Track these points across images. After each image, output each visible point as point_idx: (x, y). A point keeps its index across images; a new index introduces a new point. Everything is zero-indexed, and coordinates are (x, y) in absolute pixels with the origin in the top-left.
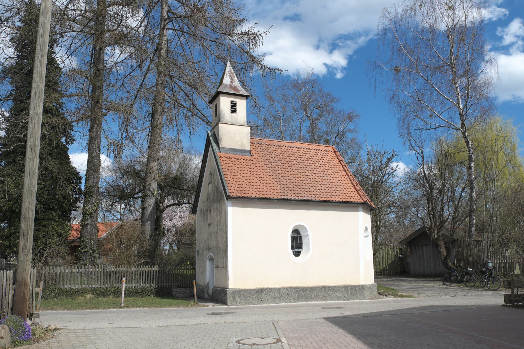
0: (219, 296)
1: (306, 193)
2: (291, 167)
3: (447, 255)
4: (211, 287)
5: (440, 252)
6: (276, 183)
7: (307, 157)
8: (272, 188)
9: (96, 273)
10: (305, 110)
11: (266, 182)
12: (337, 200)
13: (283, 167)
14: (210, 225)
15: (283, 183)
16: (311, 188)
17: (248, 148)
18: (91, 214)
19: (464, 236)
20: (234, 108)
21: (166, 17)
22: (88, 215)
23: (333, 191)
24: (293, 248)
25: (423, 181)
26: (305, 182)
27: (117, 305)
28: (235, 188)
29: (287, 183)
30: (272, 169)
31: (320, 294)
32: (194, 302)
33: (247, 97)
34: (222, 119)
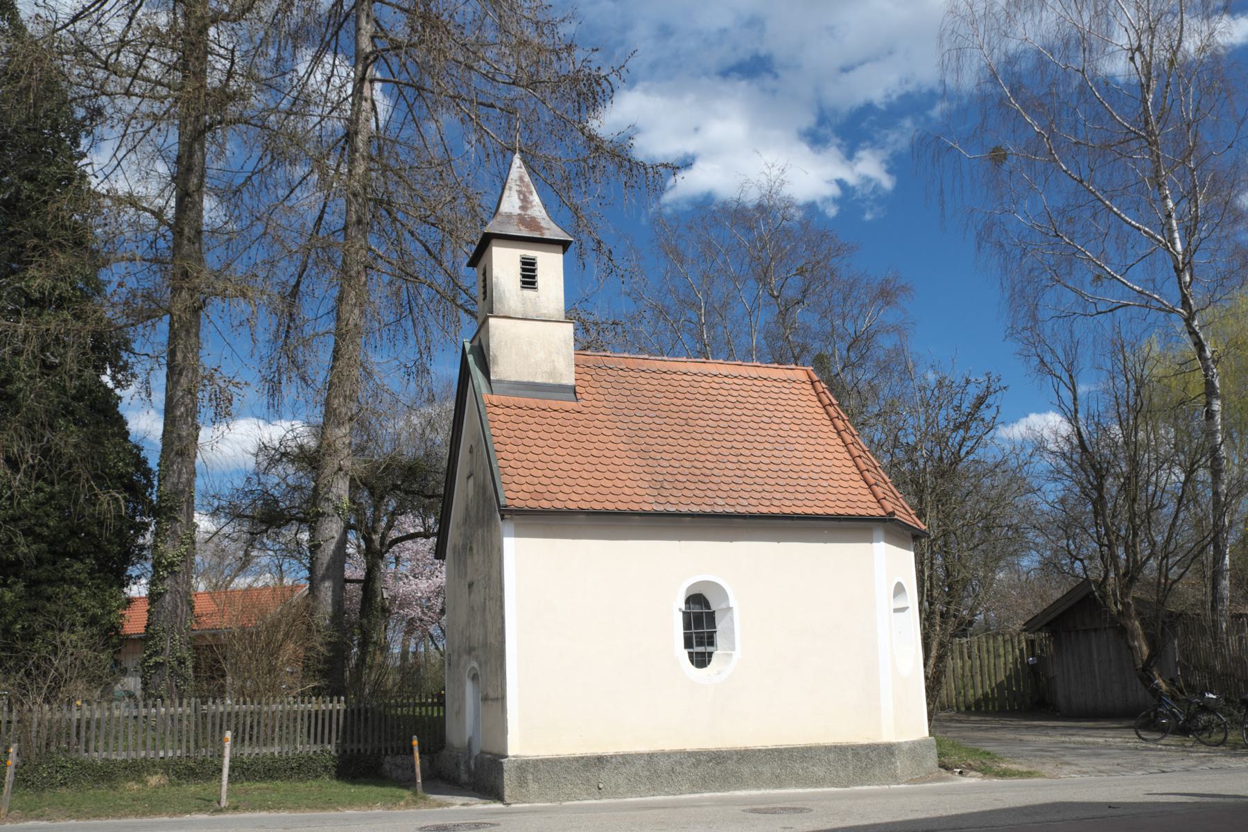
0: (482, 776)
1: (724, 495)
2: (686, 428)
3: (1151, 657)
4: (476, 752)
5: (1131, 648)
6: (640, 470)
7: (733, 399)
8: (629, 483)
9: (241, 714)
10: (763, 278)
11: (611, 467)
12: (809, 511)
13: (664, 427)
14: (471, 585)
15: (659, 469)
16: (736, 480)
17: (569, 379)
18: (172, 564)
19: (1203, 603)
20: (529, 276)
21: (369, 49)
22: (166, 568)
23: (799, 488)
24: (688, 644)
25: (1086, 460)
26: (722, 466)
27: (209, 804)
28: (525, 487)
29: (670, 470)
30: (633, 434)
32: (415, 793)
33: (564, 245)
34: (496, 306)
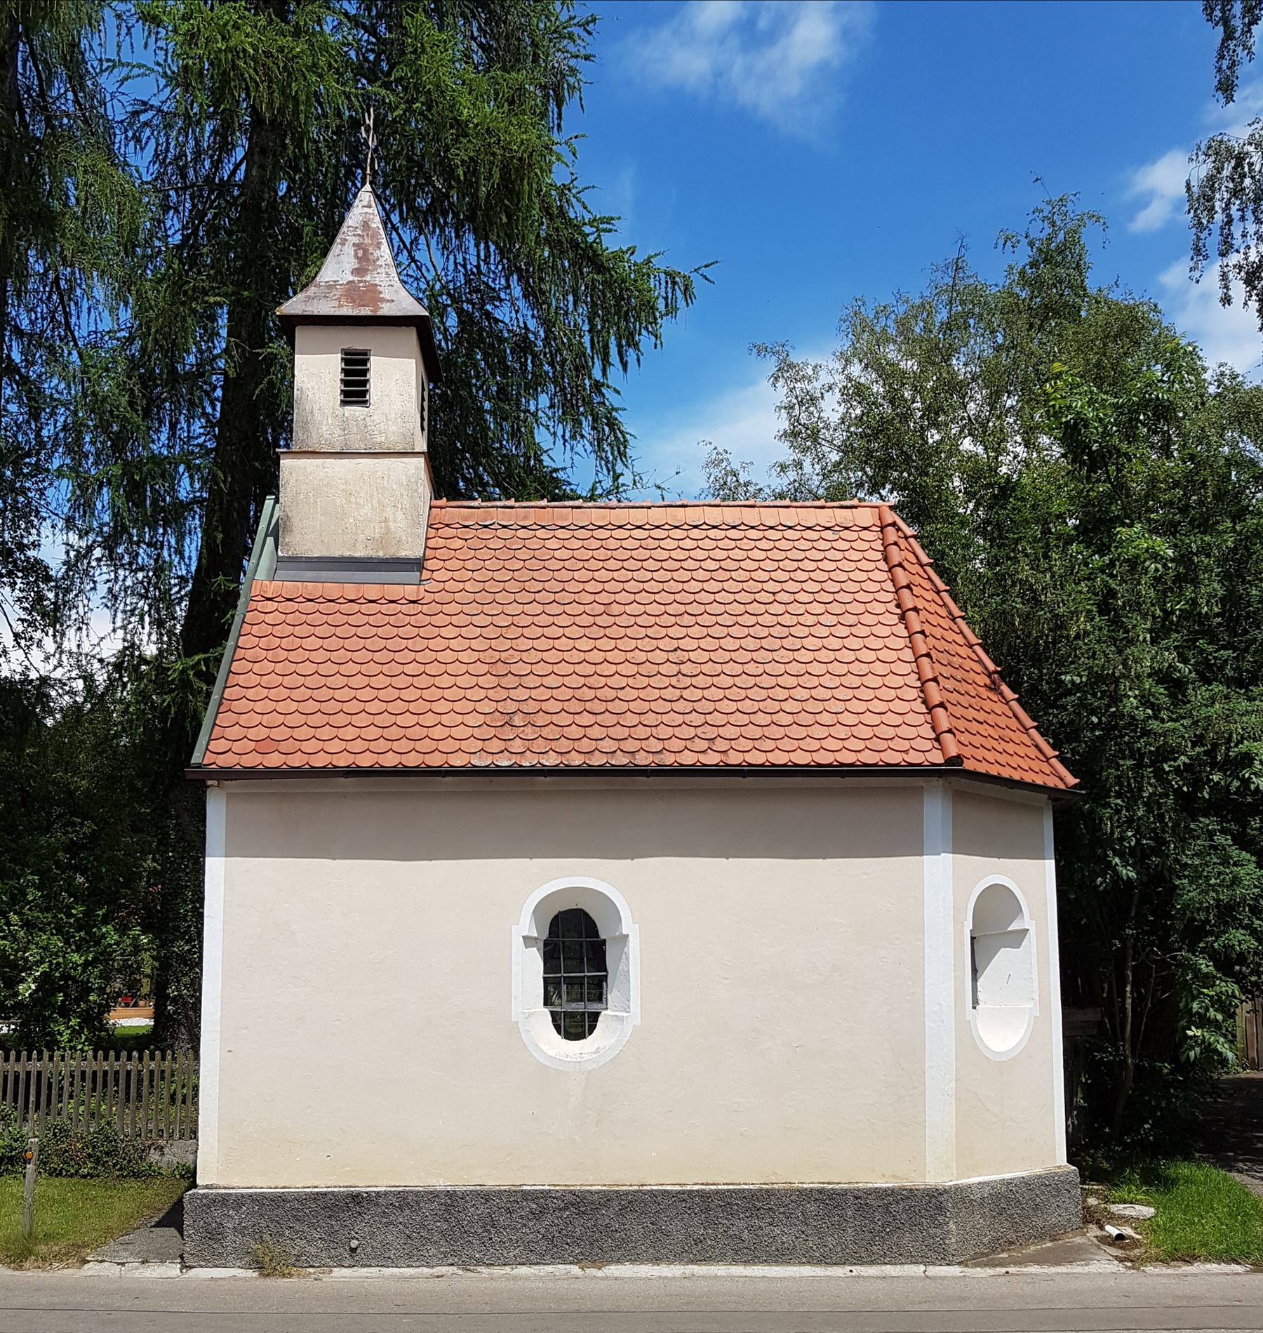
20: (355, 388)
31: (677, 1228)
34: (298, 434)
